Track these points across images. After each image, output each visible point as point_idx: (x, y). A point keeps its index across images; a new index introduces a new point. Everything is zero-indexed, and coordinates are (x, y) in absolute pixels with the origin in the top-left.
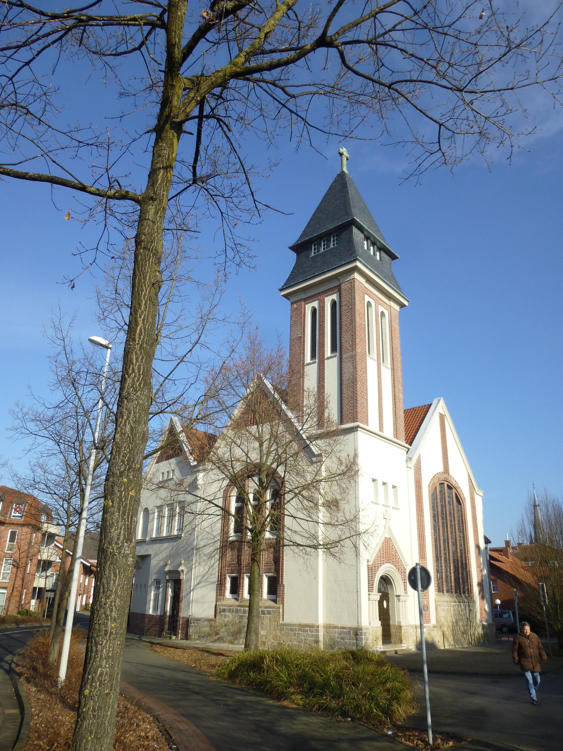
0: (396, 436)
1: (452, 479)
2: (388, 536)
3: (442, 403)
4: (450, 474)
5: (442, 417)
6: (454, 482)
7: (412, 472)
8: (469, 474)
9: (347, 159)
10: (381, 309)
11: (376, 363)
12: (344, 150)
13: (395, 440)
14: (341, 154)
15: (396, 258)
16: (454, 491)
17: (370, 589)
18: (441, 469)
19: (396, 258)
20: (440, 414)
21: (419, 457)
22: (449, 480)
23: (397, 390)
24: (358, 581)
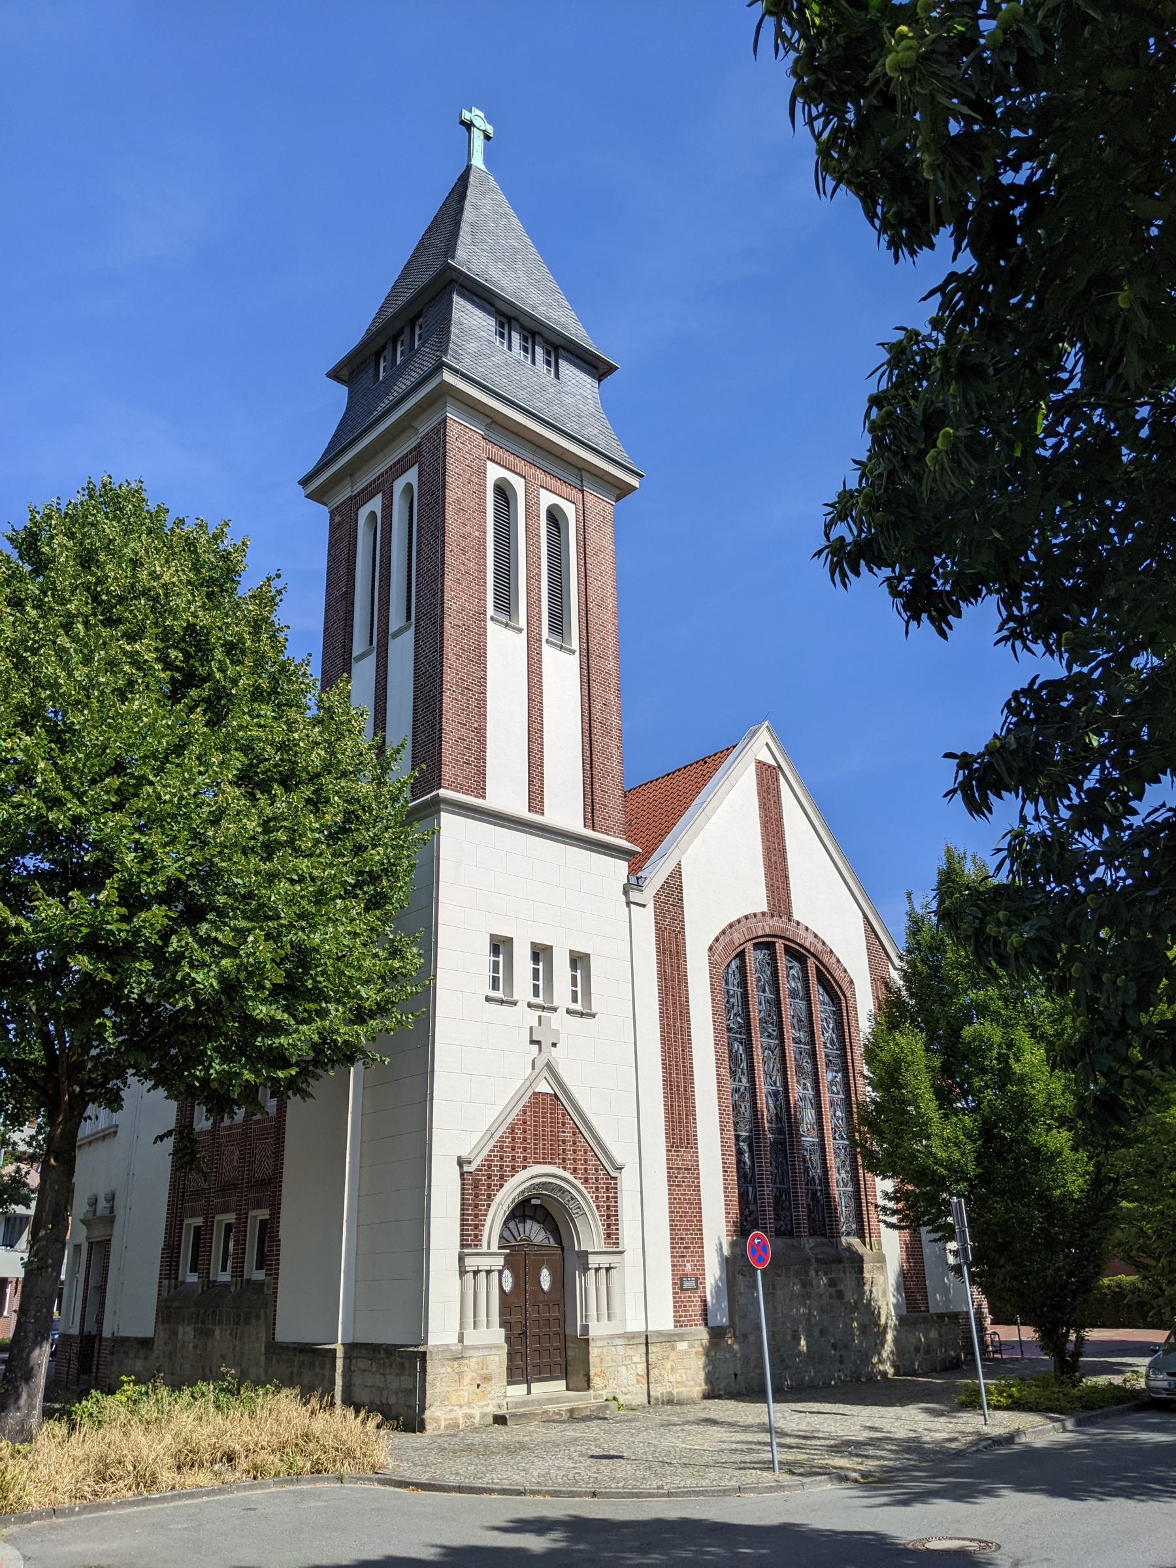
0: (591, 820)
1: (802, 932)
2: (544, 1087)
3: (764, 735)
4: (796, 916)
5: (768, 778)
6: (811, 938)
7: (645, 919)
8: (865, 917)
9: (487, 137)
10: (547, 499)
11: (520, 641)
12: (476, 116)
13: (589, 833)
14: (468, 126)
15: (611, 369)
16: (811, 962)
17: (470, 1235)
18: (760, 904)
19: (611, 369)
20: (759, 762)
21: (677, 873)
22: (789, 934)
23: (597, 705)
24: (589, 802)
